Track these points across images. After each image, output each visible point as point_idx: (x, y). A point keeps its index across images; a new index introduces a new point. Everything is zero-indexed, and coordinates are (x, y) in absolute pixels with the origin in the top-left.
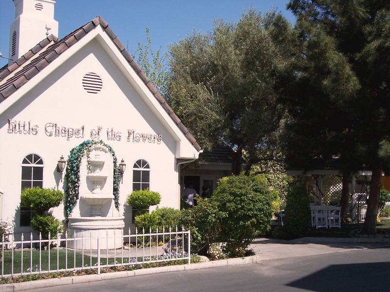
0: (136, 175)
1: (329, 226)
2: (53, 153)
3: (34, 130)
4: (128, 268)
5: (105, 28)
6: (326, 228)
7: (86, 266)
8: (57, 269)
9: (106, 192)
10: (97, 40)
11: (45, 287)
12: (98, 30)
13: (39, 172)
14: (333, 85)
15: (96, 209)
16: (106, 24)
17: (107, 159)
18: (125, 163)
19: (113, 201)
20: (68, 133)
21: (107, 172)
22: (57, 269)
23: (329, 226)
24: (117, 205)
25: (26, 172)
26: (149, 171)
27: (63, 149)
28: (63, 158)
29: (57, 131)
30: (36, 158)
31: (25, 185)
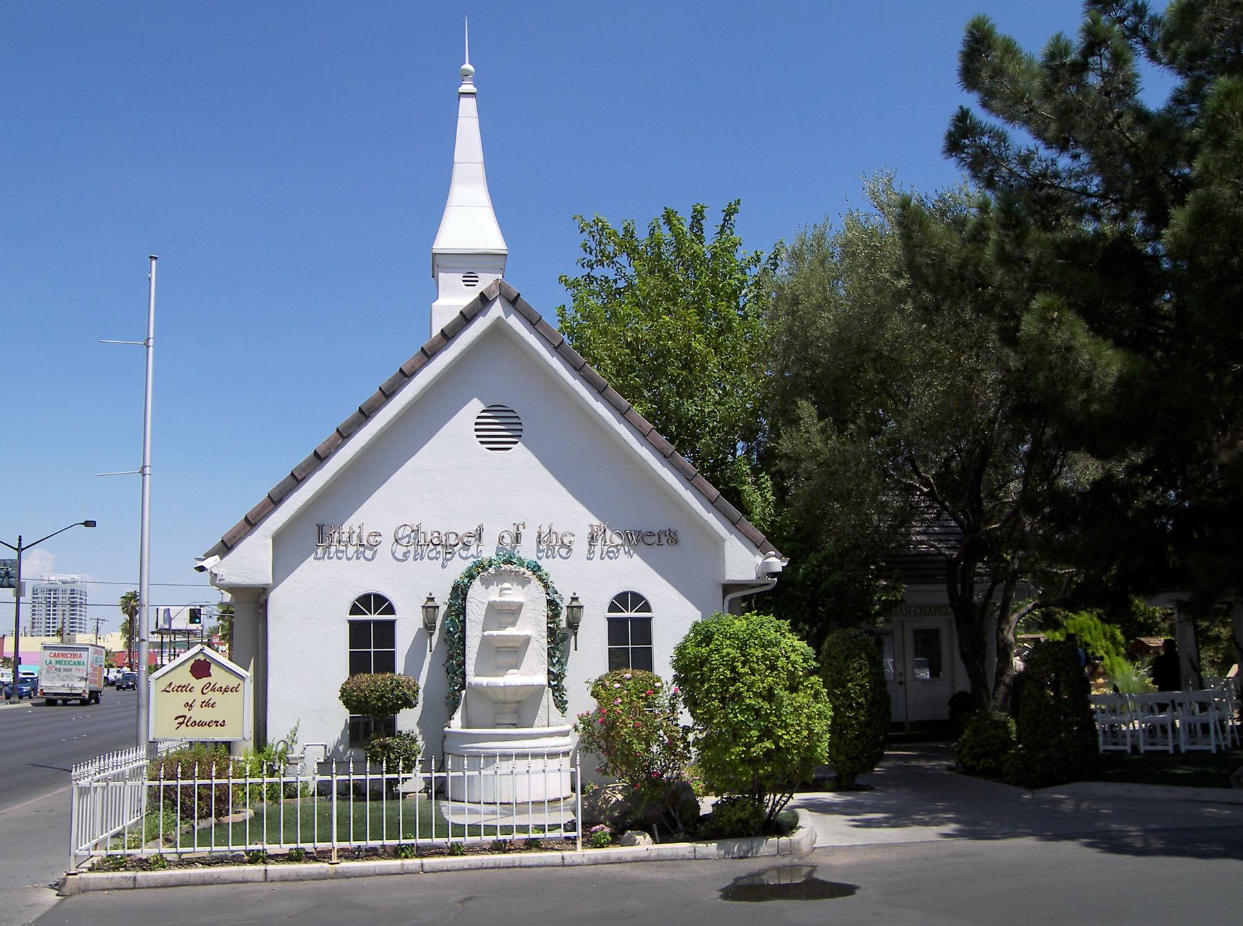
0: (617, 630)
1: (1176, 747)
2: (412, 591)
3: (367, 547)
4: (499, 847)
5: (513, 302)
6: (1210, 751)
7: (597, 844)
8: (331, 841)
9: (531, 673)
10: (498, 330)
11: (296, 880)
12: (497, 310)
13: (386, 632)
14: (822, 424)
15: (518, 709)
16: (515, 290)
17: (530, 598)
18: (581, 602)
19: (548, 696)
20: (446, 547)
21: (531, 627)
22: (331, 841)
23: (1176, 747)
24: (561, 705)
25: (358, 633)
26: (650, 619)
27: (437, 579)
28: (433, 599)
29: (417, 542)
30: (376, 601)
31: (358, 664)
